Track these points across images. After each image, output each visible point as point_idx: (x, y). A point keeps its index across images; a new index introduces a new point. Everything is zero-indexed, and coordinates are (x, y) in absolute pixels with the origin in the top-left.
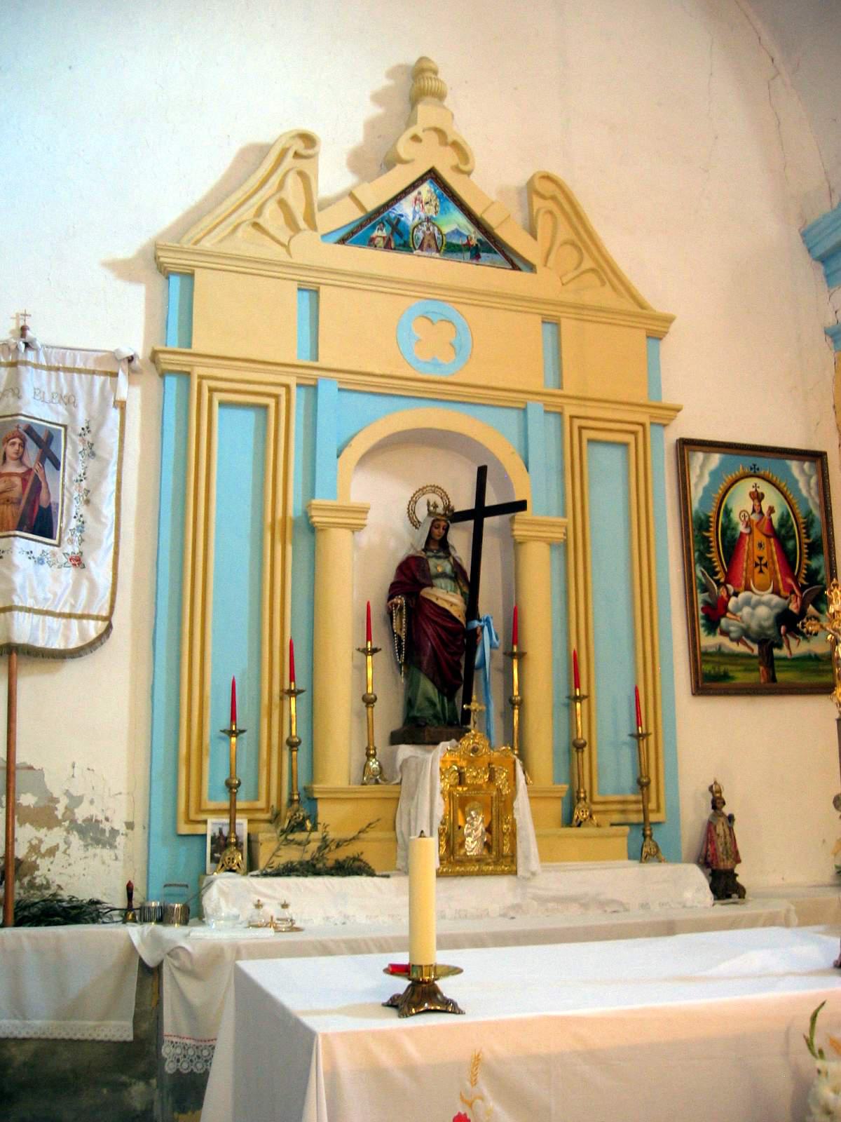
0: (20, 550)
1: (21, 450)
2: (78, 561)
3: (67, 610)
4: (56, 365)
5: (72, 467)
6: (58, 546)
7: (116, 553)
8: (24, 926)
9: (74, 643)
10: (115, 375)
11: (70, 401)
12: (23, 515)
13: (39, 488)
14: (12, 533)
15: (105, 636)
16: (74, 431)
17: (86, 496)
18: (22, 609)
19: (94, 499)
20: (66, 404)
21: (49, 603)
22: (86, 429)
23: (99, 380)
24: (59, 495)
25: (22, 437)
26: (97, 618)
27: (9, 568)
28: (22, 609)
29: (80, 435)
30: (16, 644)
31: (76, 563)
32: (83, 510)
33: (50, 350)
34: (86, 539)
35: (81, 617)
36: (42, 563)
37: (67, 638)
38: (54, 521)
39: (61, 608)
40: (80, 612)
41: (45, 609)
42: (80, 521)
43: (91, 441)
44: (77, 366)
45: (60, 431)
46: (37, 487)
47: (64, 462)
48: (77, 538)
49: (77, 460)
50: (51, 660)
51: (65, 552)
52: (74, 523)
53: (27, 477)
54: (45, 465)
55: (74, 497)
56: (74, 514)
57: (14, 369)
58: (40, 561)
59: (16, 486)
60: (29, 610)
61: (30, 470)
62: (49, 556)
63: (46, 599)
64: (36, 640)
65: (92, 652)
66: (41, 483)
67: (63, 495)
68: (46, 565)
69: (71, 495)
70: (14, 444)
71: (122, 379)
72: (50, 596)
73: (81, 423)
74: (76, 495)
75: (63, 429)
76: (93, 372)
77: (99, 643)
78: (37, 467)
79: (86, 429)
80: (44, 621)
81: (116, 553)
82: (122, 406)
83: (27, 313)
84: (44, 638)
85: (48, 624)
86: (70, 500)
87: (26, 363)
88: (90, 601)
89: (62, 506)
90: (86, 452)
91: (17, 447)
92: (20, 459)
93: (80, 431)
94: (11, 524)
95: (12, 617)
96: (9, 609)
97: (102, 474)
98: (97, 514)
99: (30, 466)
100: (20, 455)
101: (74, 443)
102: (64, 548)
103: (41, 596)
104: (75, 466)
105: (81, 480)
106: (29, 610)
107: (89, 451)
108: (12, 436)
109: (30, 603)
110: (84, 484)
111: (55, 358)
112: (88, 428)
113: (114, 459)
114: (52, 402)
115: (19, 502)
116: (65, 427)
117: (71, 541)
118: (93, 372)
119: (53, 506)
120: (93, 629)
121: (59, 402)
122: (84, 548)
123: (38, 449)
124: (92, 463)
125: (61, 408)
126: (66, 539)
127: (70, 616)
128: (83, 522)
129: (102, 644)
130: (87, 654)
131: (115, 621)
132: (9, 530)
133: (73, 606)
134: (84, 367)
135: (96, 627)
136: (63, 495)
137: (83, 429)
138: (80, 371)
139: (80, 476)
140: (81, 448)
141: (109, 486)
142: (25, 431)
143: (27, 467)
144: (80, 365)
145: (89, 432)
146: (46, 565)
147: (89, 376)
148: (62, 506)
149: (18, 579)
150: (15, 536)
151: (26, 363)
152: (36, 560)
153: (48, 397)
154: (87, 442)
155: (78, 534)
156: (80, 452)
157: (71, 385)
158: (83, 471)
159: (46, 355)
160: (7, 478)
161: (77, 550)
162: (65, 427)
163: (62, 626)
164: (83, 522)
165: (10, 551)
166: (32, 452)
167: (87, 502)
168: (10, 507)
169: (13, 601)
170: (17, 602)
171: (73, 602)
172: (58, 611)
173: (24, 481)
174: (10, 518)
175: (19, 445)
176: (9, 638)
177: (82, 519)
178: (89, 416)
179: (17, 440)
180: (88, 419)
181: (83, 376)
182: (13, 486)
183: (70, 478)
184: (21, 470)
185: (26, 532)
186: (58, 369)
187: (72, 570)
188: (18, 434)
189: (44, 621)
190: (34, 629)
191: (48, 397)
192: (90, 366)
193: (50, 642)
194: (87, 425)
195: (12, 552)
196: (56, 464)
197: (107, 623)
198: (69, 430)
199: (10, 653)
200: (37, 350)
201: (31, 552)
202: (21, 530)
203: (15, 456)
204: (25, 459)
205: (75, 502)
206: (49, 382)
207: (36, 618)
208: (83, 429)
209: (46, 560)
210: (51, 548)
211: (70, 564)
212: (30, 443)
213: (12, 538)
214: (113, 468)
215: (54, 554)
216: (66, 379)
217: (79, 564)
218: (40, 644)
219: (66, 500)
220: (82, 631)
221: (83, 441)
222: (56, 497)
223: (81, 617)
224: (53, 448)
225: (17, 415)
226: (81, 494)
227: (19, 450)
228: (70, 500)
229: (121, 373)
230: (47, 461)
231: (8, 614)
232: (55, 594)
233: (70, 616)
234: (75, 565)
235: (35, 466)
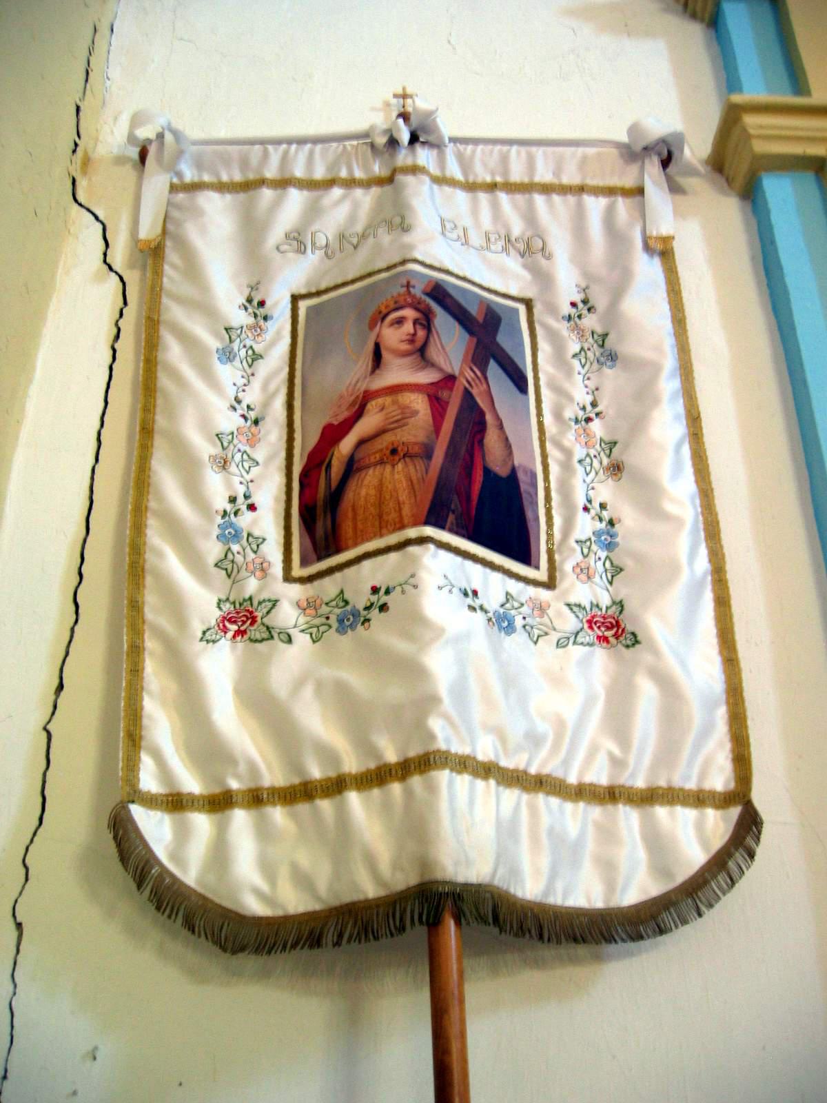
0: (442, 582)
1: (421, 333)
2: (613, 629)
3: (600, 775)
4: (488, 179)
5: (557, 390)
6: (550, 584)
7: (722, 603)
8: (220, 906)
9: (637, 888)
10: (640, 191)
11: (532, 249)
12: (442, 487)
13: (481, 426)
14: (412, 533)
15: (739, 856)
16: (552, 309)
17: (609, 456)
18: (464, 764)
19: (632, 458)
20: (522, 256)
21: (544, 753)
22: (581, 305)
23: (595, 206)
24: (533, 451)
25: (422, 307)
26: (699, 799)
27: (408, 636)
28: (464, 764)
29: (569, 318)
30: (454, 884)
31: (609, 634)
32: (605, 491)
33: (470, 148)
34: (628, 563)
35: (648, 798)
36: (510, 629)
37: (608, 868)
38: (529, 514)
39: (581, 773)
40: (640, 783)
41: (533, 771)
42: (601, 520)
43: (599, 330)
44: (537, 179)
45: (516, 311)
46: (474, 422)
47: (536, 378)
48: (600, 564)
49: (569, 372)
50: (567, 949)
51: (572, 600)
52: (585, 526)
53: (444, 394)
54: (490, 374)
55: (576, 458)
56: (581, 501)
57: (388, 189)
58: (503, 622)
59: (415, 413)
60: (486, 770)
61: (449, 380)
62: (525, 610)
63: (534, 740)
64: (515, 872)
65: (751, 855)
66: (482, 414)
67: (544, 456)
68: (519, 637)
69: (568, 453)
70: (400, 321)
71: (656, 193)
72: (543, 727)
73: (567, 285)
74: (579, 452)
75: (522, 308)
76: (581, 189)
77: (722, 878)
78: (469, 374)
79: (581, 305)
80: (534, 811)
81: (722, 603)
82: (663, 251)
83: (409, 91)
84: (537, 872)
85: (545, 820)
86: (567, 467)
87: (415, 170)
88: (668, 751)
89: (546, 479)
90: (590, 354)
91: (408, 327)
92: (420, 352)
93: (566, 309)
94: (406, 511)
95: (432, 789)
96: (425, 762)
97: (645, 396)
98: (649, 496)
99: (449, 370)
100: (419, 344)
101: (554, 336)
102: (566, 592)
103: (516, 731)
104: (567, 386)
105: (588, 420)
106: (486, 770)
107: (598, 351)
108: (392, 306)
109: (485, 750)
110: (596, 427)
111: (484, 164)
112: (585, 302)
113: (669, 362)
114: (488, 248)
115: (427, 453)
116: (528, 303)
117: (585, 572)
118: (581, 189)
119: (521, 476)
120: (694, 837)
121: (505, 250)
122: (623, 590)
123: (467, 336)
124: (611, 377)
125: (513, 263)
126: (568, 567)
127: (611, 795)
128: (611, 523)
129: (733, 882)
130: (684, 922)
131: (759, 798)
132: (402, 527)
133: (617, 763)
134: (556, 181)
135: (700, 826)
136: (544, 456)
137: (573, 305)
138: (547, 189)
139: (584, 408)
140: (576, 348)
141: (666, 426)
142: (428, 294)
143: (440, 370)
144: (544, 174)
145: (589, 310)
146: (519, 637)
147: (571, 199)
148: (546, 479)
149: (440, 664)
150: (422, 541)
151: (415, 170)
152: (490, 615)
153: (476, 239)
154: (588, 334)
155: (603, 554)
156: (575, 356)
157: (530, 218)
158: (589, 399)
159: (460, 158)
160: (388, 400)
161: (605, 601)
162: (528, 303)
163: (591, 830)
164: (611, 523)
165: (411, 583)
166: (451, 346)
167: (616, 469)
168: (400, 466)
169: (432, 737)
170: (444, 736)
171: (617, 751)
172: (572, 779)
173: (438, 406)
174: (403, 496)
175: (415, 322)
176: (425, 863)
177: (605, 514)
178: (586, 274)
179: (409, 313)
180: (583, 285)
181: (556, 198)
182: (407, 414)
183: (558, 416)
184: (426, 377)
185: (451, 531)
186: (492, 187)
187: (600, 655)
188: (409, 300)
189: (534, 811)
190: (507, 831)
191: (476, 239)
192: (570, 177)
193: (559, 886)
194: (582, 296)
195: (415, 587)
196: (519, 381)
197: (735, 812)
198: (538, 309)
199: (434, 924)
200: (437, 145)
201: (475, 593)
202: (441, 525)
203: (405, 347)
204: (433, 353)
205: (580, 470)
206: (475, 211)
207: (511, 797)
208: (573, 305)
209: (519, 622)
210: (532, 591)
211: (589, 636)
212: (442, 319)
213: (412, 549)
214: (669, 385)
215: (542, 609)
216: (515, 206)
217: (616, 636)
218: (530, 887)
219: (554, 469)
220: (657, 844)
221: (580, 332)
222: (527, 456)
223: (648, 798)
224: (502, 339)
225: (404, 262)
226: (592, 452)
227: (414, 334)
228: (567, 467)
229: (650, 188)
230: (493, 369)
231: (416, 781)
232: (560, 725)
233: (611, 795)
234: (606, 639)
235: (461, 373)
